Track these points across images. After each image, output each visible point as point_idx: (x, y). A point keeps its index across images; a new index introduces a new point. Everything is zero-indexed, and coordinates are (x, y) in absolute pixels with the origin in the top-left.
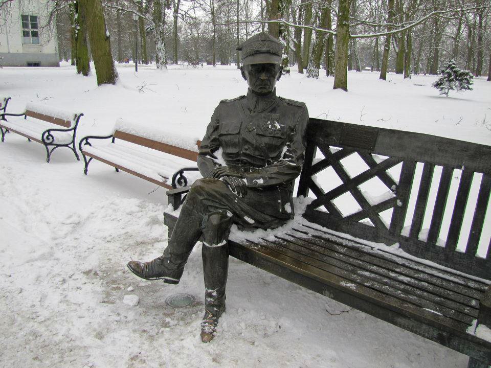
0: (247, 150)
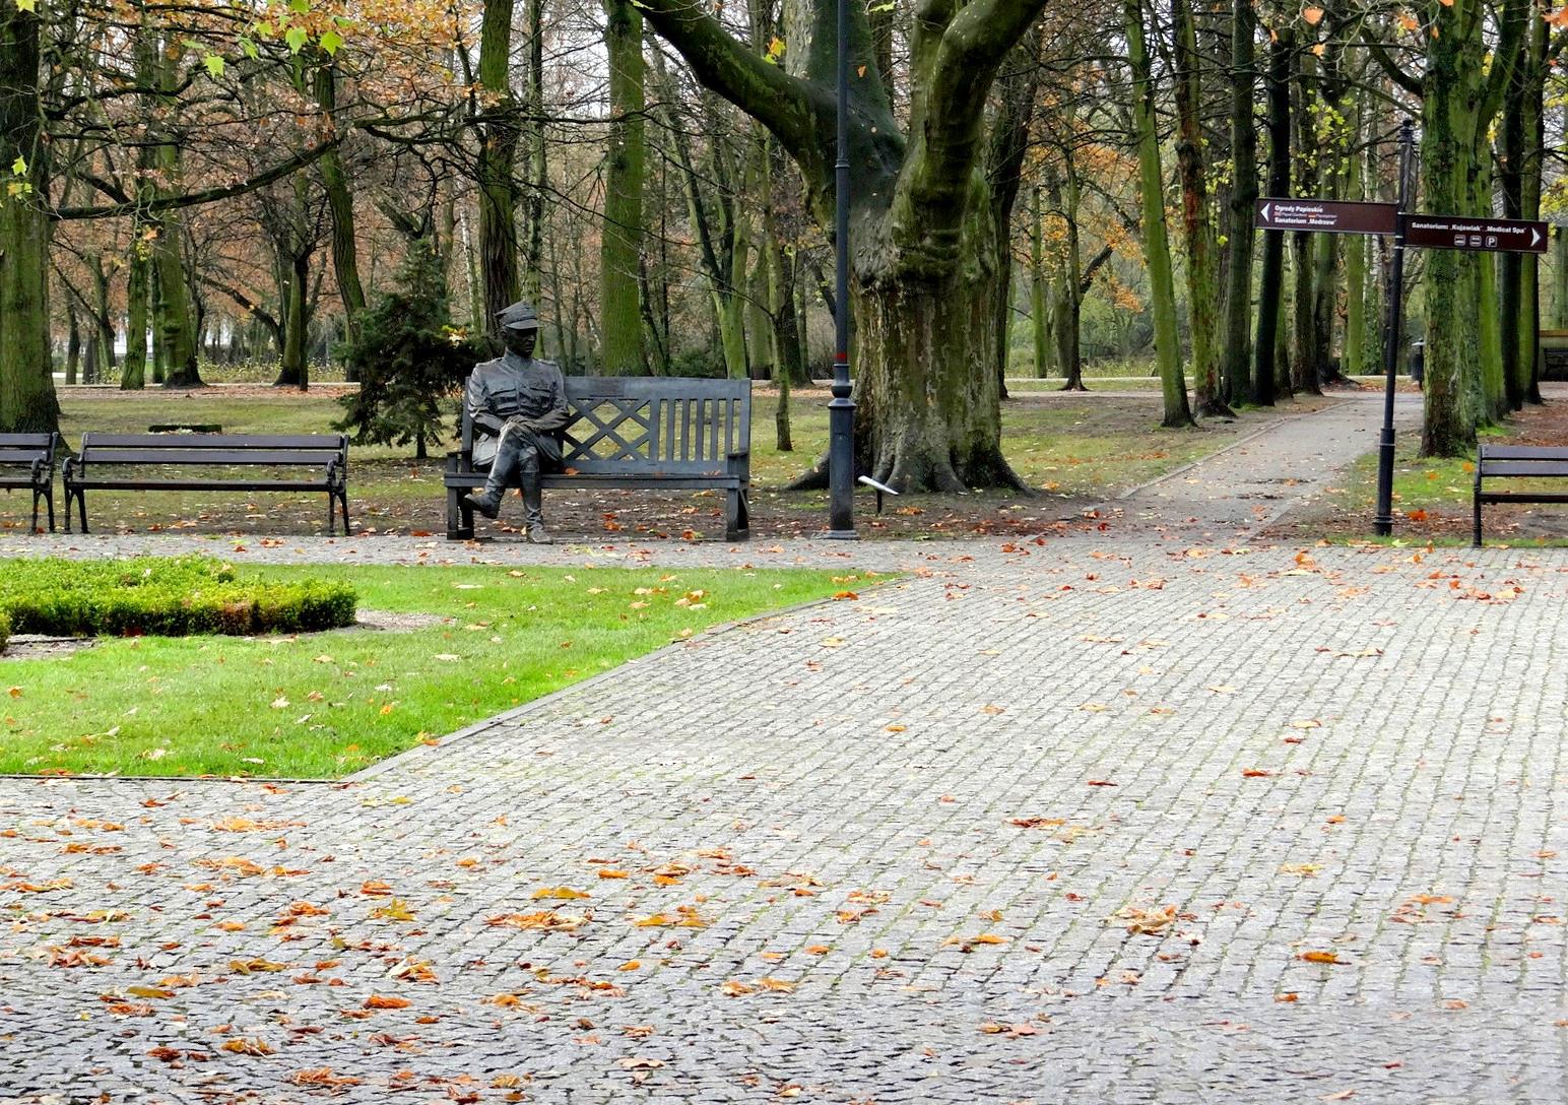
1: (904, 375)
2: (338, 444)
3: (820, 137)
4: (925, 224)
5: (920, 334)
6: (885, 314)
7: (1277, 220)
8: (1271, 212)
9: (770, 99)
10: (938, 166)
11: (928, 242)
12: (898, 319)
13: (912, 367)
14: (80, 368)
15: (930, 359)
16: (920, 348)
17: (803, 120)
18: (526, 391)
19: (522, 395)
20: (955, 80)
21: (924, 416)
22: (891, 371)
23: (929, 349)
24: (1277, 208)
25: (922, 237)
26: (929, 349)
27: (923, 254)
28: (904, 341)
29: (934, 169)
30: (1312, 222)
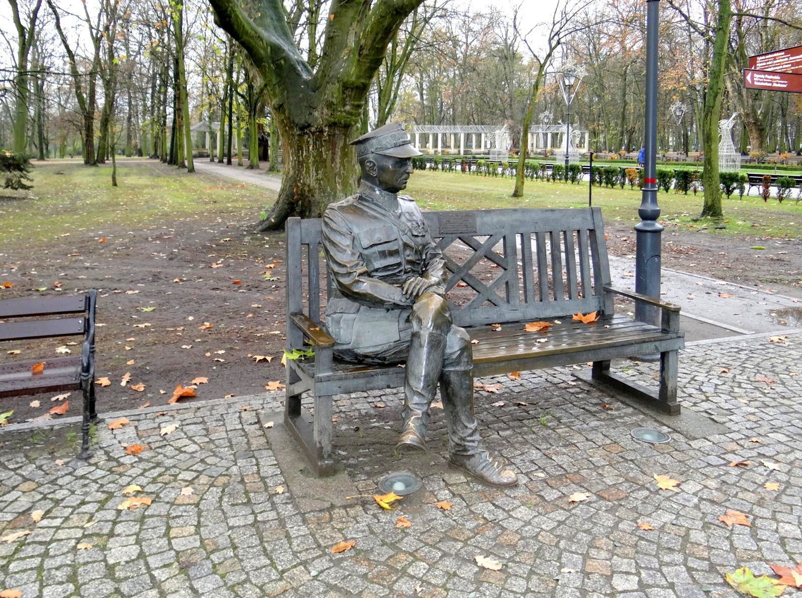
1: (324, 173)
2: (81, 306)
3: (272, 59)
4: (348, 99)
5: (334, 153)
6: (315, 144)
7: (756, 83)
8: (752, 78)
9: (253, 37)
10: (364, 68)
11: (348, 108)
12: (322, 146)
13: (329, 169)
14: (519, 246)
15: (338, 166)
16: (333, 160)
17: (265, 49)
18: (406, 239)
19: (406, 245)
20: (386, 23)
21: (335, 193)
22: (317, 171)
23: (338, 160)
24: (755, 75)
25: (344, 105)
26: (338, 160)
27: (344, 114)
28: (325, 157)
29: (360, 70)
30: (775, 85)
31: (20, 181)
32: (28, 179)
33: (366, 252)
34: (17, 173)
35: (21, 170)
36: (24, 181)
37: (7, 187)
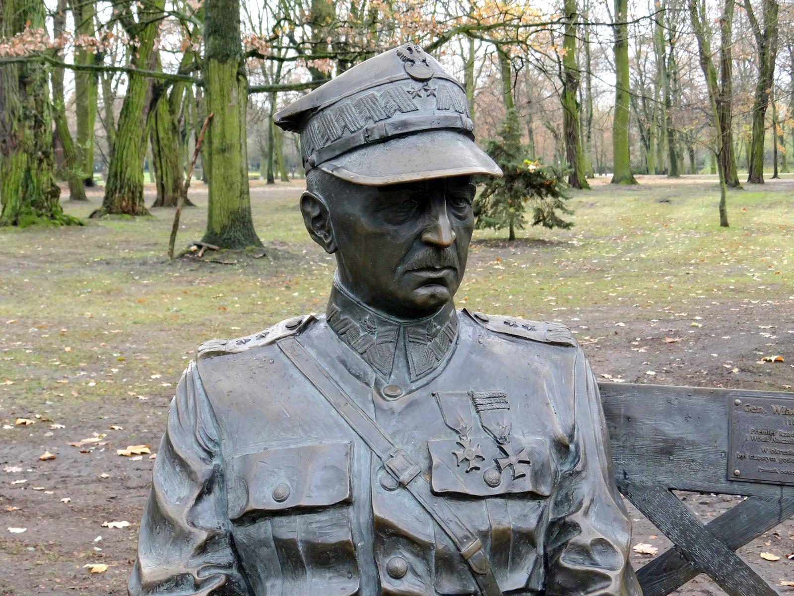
0: (397, 575)
31: (553, 213)
32: (565, 211)
33: (240, 534)
34: (549, 199)
35: (555, 194)
36: (558, 213)
37: (536, 223)
